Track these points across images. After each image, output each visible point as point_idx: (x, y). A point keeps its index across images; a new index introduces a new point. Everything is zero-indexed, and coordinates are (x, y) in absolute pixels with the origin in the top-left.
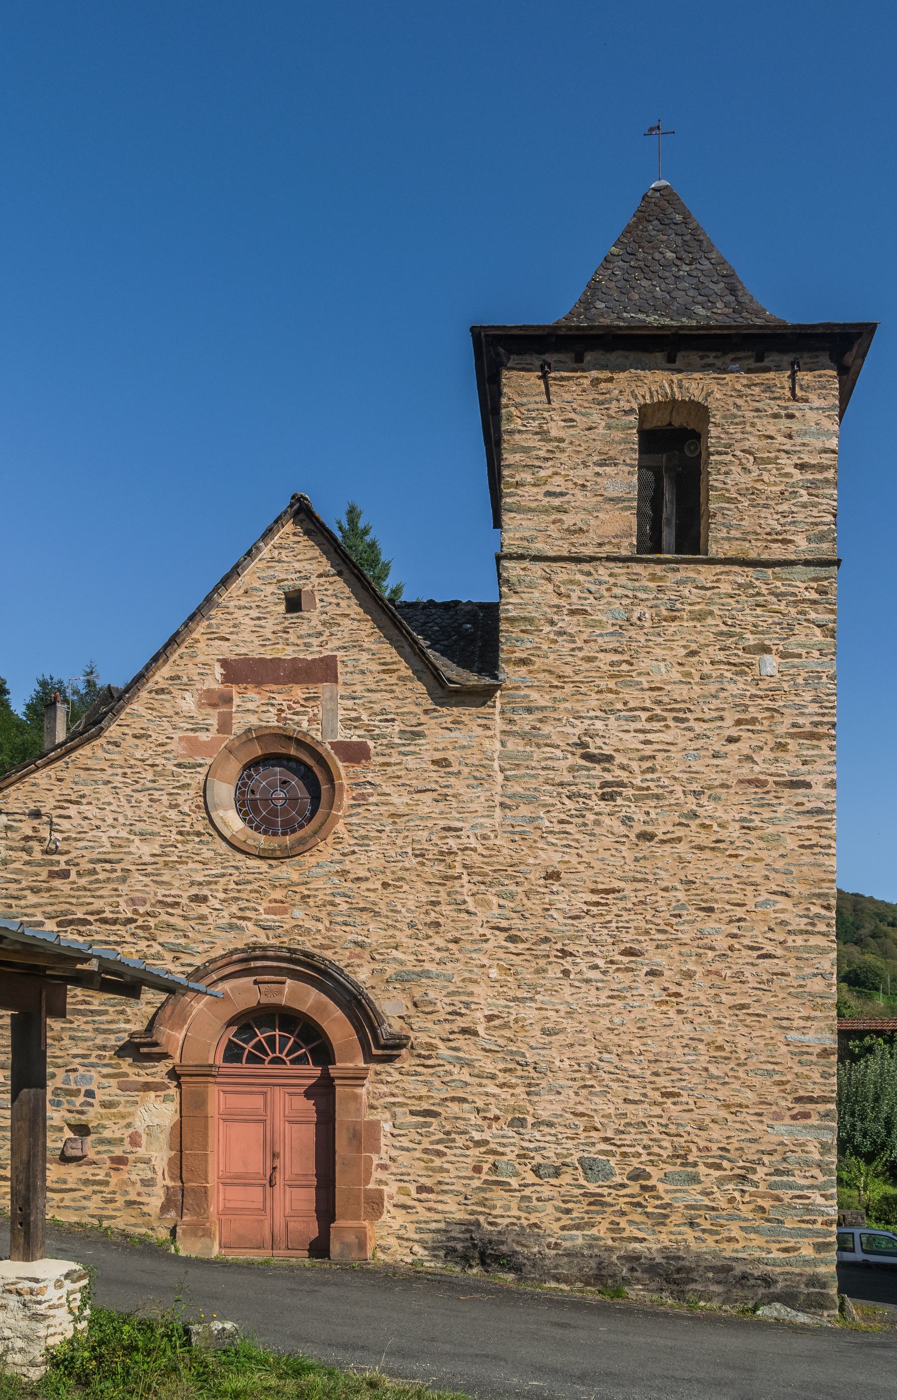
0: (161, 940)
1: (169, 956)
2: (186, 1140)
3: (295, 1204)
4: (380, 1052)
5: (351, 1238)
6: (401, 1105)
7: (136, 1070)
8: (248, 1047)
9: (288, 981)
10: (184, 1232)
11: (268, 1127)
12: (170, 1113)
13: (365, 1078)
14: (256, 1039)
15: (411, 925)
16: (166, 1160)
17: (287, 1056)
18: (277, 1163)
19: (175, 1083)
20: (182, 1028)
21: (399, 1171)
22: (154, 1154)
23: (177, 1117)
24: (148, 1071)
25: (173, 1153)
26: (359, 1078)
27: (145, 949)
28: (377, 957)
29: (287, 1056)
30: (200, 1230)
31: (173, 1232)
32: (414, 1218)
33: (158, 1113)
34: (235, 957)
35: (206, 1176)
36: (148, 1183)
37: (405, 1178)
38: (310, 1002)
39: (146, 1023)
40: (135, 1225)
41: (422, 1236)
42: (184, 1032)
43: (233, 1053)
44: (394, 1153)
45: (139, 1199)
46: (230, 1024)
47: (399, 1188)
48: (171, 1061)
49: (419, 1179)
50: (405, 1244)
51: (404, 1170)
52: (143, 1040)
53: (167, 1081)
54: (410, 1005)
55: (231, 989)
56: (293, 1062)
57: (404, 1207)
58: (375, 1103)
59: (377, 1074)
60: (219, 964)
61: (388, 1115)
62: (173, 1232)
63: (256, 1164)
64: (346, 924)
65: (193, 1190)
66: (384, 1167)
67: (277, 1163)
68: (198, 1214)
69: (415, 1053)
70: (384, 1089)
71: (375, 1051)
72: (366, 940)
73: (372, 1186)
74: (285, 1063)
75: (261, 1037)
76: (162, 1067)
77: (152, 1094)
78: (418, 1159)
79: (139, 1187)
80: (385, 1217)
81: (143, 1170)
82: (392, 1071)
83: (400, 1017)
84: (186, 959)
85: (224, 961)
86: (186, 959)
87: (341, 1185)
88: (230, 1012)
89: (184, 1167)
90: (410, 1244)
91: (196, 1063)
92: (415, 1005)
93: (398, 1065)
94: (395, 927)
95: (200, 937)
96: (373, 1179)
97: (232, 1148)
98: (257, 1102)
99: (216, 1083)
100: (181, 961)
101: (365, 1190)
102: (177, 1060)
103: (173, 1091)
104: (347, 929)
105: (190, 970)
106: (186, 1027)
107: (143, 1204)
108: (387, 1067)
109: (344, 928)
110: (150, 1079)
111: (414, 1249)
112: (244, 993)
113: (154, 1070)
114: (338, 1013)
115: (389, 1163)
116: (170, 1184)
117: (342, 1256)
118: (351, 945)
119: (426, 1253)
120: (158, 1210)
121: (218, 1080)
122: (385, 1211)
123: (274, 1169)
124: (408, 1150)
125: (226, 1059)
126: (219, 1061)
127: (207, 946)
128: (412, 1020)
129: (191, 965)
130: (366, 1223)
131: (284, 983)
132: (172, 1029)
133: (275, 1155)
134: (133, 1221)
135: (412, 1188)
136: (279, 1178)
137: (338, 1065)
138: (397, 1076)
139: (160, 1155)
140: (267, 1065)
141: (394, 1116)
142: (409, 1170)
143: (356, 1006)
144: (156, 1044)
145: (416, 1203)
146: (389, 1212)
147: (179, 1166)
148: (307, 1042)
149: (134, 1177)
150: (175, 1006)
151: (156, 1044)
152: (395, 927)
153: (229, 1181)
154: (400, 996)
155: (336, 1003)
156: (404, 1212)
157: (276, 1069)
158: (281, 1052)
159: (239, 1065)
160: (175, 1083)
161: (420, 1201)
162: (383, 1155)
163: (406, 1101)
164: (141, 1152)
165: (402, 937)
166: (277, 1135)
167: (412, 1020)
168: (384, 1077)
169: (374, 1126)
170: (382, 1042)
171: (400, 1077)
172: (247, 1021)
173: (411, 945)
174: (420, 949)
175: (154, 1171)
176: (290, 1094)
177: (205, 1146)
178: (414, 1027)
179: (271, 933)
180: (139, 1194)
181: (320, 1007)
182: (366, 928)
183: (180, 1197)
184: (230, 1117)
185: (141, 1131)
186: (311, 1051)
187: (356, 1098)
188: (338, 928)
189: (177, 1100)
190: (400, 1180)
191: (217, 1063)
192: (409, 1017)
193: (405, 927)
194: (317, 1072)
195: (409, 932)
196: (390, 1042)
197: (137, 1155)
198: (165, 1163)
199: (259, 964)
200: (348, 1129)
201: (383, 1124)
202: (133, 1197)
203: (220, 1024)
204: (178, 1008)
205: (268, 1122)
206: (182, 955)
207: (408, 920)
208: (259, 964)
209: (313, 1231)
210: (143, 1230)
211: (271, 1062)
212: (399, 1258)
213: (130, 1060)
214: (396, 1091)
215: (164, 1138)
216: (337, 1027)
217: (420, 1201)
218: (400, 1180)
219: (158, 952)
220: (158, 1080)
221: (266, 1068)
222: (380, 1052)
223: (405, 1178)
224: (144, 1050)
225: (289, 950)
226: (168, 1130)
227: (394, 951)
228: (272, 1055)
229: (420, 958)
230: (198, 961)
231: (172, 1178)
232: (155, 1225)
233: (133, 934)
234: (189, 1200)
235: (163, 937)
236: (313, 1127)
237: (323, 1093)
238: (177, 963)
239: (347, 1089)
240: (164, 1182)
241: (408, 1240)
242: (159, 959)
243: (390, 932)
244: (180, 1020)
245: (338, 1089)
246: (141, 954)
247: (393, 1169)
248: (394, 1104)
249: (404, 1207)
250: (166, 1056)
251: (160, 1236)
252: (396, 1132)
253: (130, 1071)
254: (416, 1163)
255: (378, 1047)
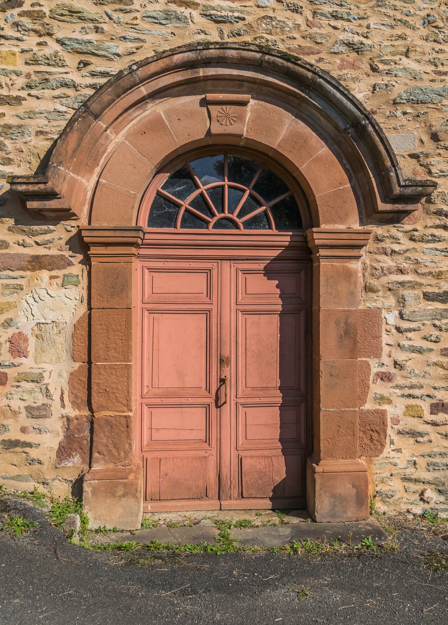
0: (60, 35)
1: (72, 61)
2: (97, 344)
3: (255, 432)
4: (388, 207)
5: (346, 488)
6: (414, 285)
7: (20, 238)
8: (186, 203)
9: (252, 102)
10: (95, 491)
11: (214, 321)
12: (72, 304)
13: (360, 247)
14: (197, 192)
15: (428, 21)
16: (66, 376)
17: (240, 215)
18: (227, 372)
19: (80, 257)
20: (91, 171)
21: (407, 382)
22: (48, 367)
23: (83, 309)
24: (39, 239)
25: (77, 365)
26: (351, 246)
27: (35, 49)
28: (381, 67)
29: (240, 215)
30: (117, 486)
31: (78, 488)
32: (426, 449)
33: (55, 303)
34: (177, 58)
35: (129, 400)
36: (37, 412)
37: (416, 392)
38: (283, 132)
39: (36, 164)
40: (17, 478)
41: (436, 474)
42: (94, 178)
43: (163, 212)
44: (401, 356)
45: (23, 438)
46: (160, 170)
47: (407, 407)
48: (74, 223)
49: (436, 393)
50: (413, 487)
51: (414, 381)
52: (31, 188)
53: (67, 254)
54: (426, 138)
55: (167, 113)
56: (248, 224)
57: (414, 434)
58: (374, 282)
59: (378, 240)
60: (153, 68)
61: (391, 301)
62: (78, 488)
63: (195, 375)
64: (335, 17)
65: (108, 422)
66: (385, 377)
67: (227, 372)
68: (116, 460)
69: (433, 208)
70: (388, 262)
71: (382, 206)
72: (365, 41)
73: (369, 406)
74: (237, 227)
75: (203, 189)
76: (59, 235)
77: (45, 274)
78: (435, 364)
79: (24, 420)
80: (388, 450)
81: (31, 392)
82: (400, 235)
83: (412, 156)
84: (99, 65)
85: (161, 64)
86: (99, 65)
87: (330, 404)
88: (164, 148)
89: (94, 387)
90: (419, 487)
91: (112, 225)
92: (435, 137)
93: (408, 227)
94: (405, 23)
95: (120, 31)
96: (370, 395)
97: (164, 352)
98: (196, 283)
99: (139, 256)
100: (90, 68)
101: (362, 412)
102: (83, 222)
103: (77, 269)
104: (339, 23)
105: (102, 81)
106: (98, 170)
107: (30, 445)
108: (393, 230)
109: (334, 23)
110: (41, 251)
111: (426, 495)
112: (185, 119)
113: (48, 237)
114: (323, 150)
115: (393, 370)
116: (72, 412)
117: (333, 516)
118: (343, 49)
119: (442, 499)
120: (54, 456)
121: (143, 252)
122: (388, 441)
123: (223, 381)
124: (420, 351)
125: (152, 222)
126: (143, 222)
127: (130, 45)
128: (431, 160)
129: (104, 74)
130: (362, 461)
131: (244, 104)
132: (77, 171)
133: (223, 361)
134: (15, 471)
135: (425, 406)
136: (229, 391)
137: (324, 227)
138: (406, 244)
139: (57, 368)
140: (211, 230)
141: (402, 301)
142: (422, 381)
143: (355, 139)
144: (52, 195)
145: (428, 428)
146: (392, 443)
147: (87, 386)
148: (268, 197)
149: (16, 404)
150: (83, 133)
151: (52, 195)
152: (405, 23)
153: (158, 401)
154: (412, 126)
155: (320, 135)
156: (412, 441)
157: (227, 236)
158: (231, 211)
159: (172, 230)
160: (80, 257)
161: (434, 424)
162: (385, 359)
163: (418, 279)
164: (28, 364)
165: (415, 38)
166: (226, 331)
167: (431, 160)
168: (388, 245)
169: (373, 317)
170: (397, 190)
171: (412, 245)
172: (179, 167)
173: (427, 50)
174: (440, 56)
175: (48, 394)
176: (246, 272)
177: (126, 354)
178: (434, 170)
179: (226, 28)
180: (23, 430)
181: (296, 139)
182: (364, 23)
183: (87, 433)
184: (160, 307)
185: (27, 332)
186: (274, 209)
187: (349, 275)
188: (324, 22)
189: (84, 282)
190: (409, 396)
191: (141, 224)
192: (427, 156)
193: (419, 24)
194: (285, 238)
195: (424, 32)
196: (408, 191)
197: (21, 369)
198: (64, 382)
199: (211, 71)
200: (337, 323)
201: (384, 313)
202: (14, 434)
203: (150, 167)
204: (87, 137)
205: (214, 313)
206: (92, 59)
207: (423, 13)
208: (211, 71)
209: (279, 470)
210: (30, 486)
211: (216, 226)
212: (404, 507)
213: (11, 222)
214: (405, 265)
215: (62, 342)
216: (321, 170)
217: (434, 424)
218: (409, 396)
219: (56, 54)
220: (54, 252)
221: (210, 234)
222: (388, 207)
223: (416, 392)
224: (32, 205)
225: (261, 49)
226: (69, 329)
227: (404, 59)
228: (219, 216)
229: (440, 68)
230: (114, 68)
231: (74, 404)
232: (48, 477)
233: (16, 25)
234: (101, 439)
235: (63, 31)
236: (276, 319)
237: (298, 273)
238: (85, 71)
239: (337, 263)
240: (64, 409)
241: (416, 481)
242: (56, 65)
243: (399, 31)
244: (89, 157)
245: (323, 263)
246: (28, 56)
247: (400, 381)
248: (402, 284)
249: (414, 434)
250: (66, 214)
251: (56, 493)
252: (405, 325)
253: (11, 238)
254: (432, 370)
255: (388, 197)
